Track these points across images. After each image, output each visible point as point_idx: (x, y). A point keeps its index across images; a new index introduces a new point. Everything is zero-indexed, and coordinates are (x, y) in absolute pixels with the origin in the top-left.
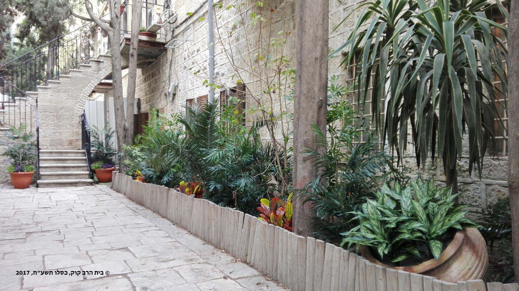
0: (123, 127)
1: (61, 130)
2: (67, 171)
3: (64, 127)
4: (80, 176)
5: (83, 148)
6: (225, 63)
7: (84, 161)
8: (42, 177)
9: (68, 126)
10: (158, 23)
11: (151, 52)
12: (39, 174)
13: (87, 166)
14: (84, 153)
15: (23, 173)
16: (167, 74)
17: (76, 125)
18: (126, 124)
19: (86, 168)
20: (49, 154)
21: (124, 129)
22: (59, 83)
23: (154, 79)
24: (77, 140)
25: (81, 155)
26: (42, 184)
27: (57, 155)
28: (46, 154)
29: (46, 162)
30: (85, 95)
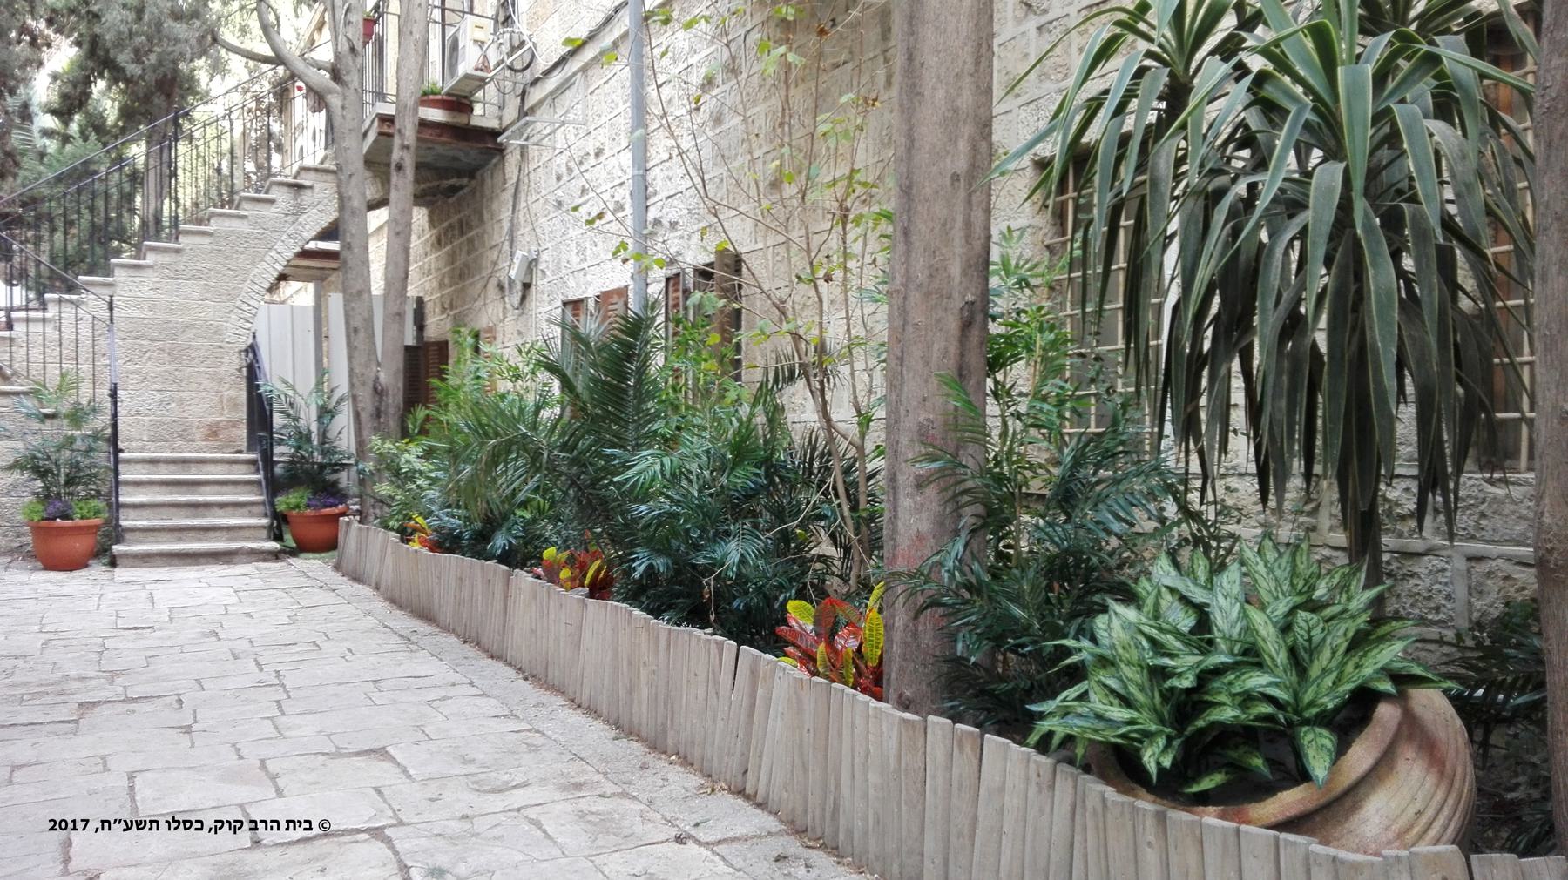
0: (371, 384)
2: (204, 516)
3: (194, 385)
4: (242, 533)
5: (250, 449)
6: (680, 189)
7: (255, 488)
8: (128, 536)
9: (206, 382)
10: (476, 69)
11: (455, 159)
12: (118, 525)
13: (263, 503)
14: (253, 462)
15: (68, 523)
17: (228, 379)
18: (382, 375)
19: (261, 509)
20: (147, 466)
21: (375, 389)
22: (177, 251)
23: (465, 238)
24: (234, 424)
25: (244, 468)
26: (126, 555)
27: (172, 468)
28: (139, 466)
29: (140, 489)
30: (256, 288)
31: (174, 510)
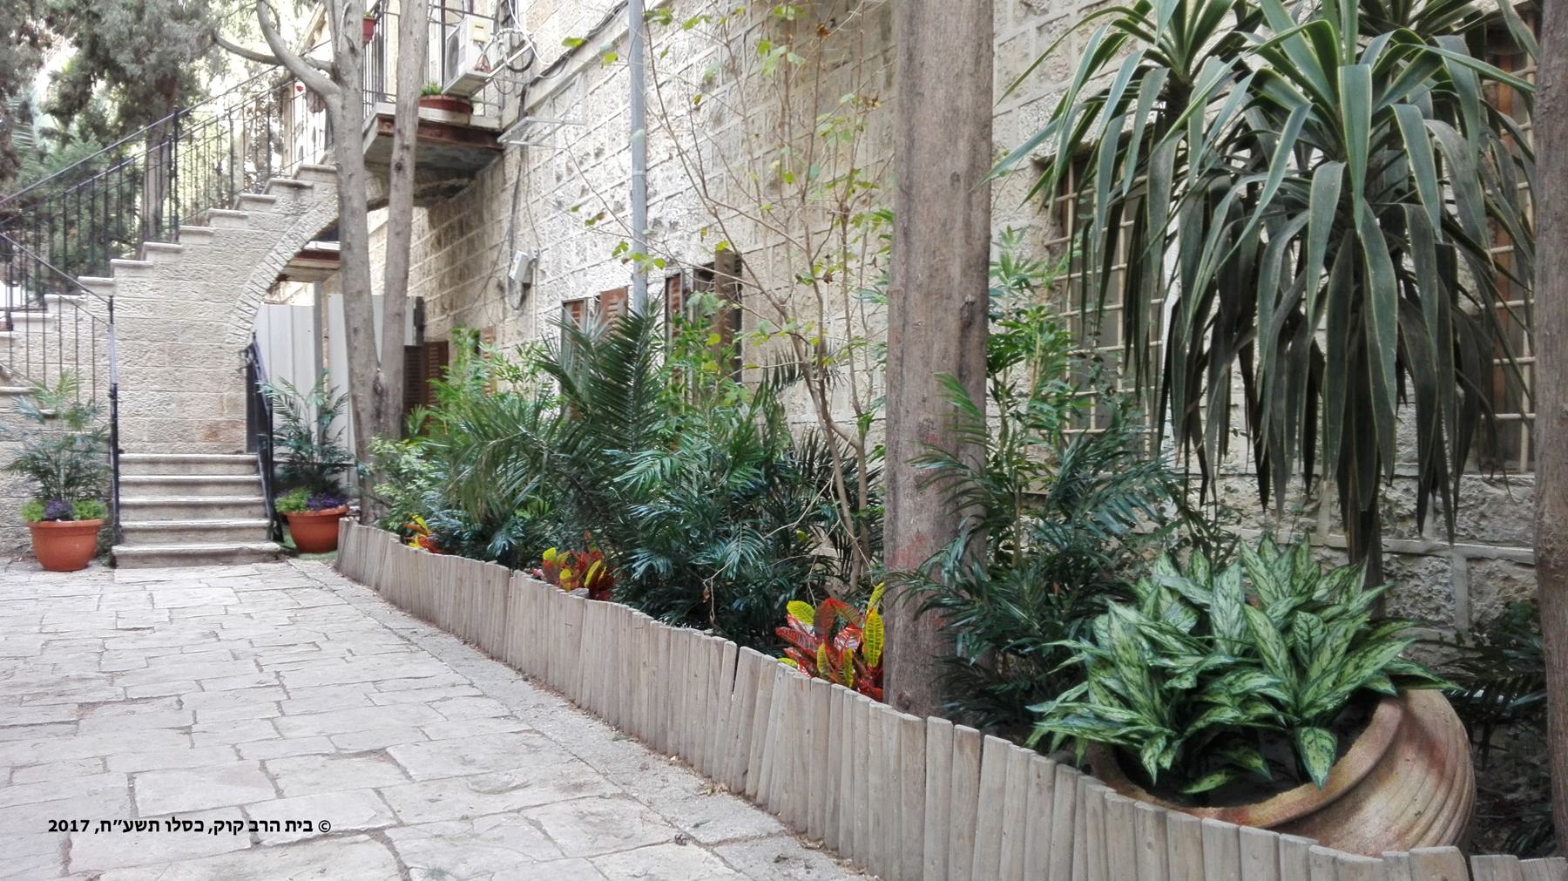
0: (370, 384)
1: (183, 395)
2: (204, 517)
4: (242, 534)
5: (250, 449)
7: (255, 488)
8: (128, 537)
9: (206, 383)
10: (476, 69)
12: (118, 526)
13: (263, 504)
14: (253, 463)
15: (69, 523)
16: (506, 225)
17: (228, 380)
18: (382, 376)
19: (261, 510)
20: (147, 467)
21: (375, 390)
22: (177, 251)
24: (234, 424)
25: (244, 468)
26: (126, 556)
27: (172, 468)
28: (139, 467)
29: (139, 490)
30: (256, 288)
31: (174, 511)
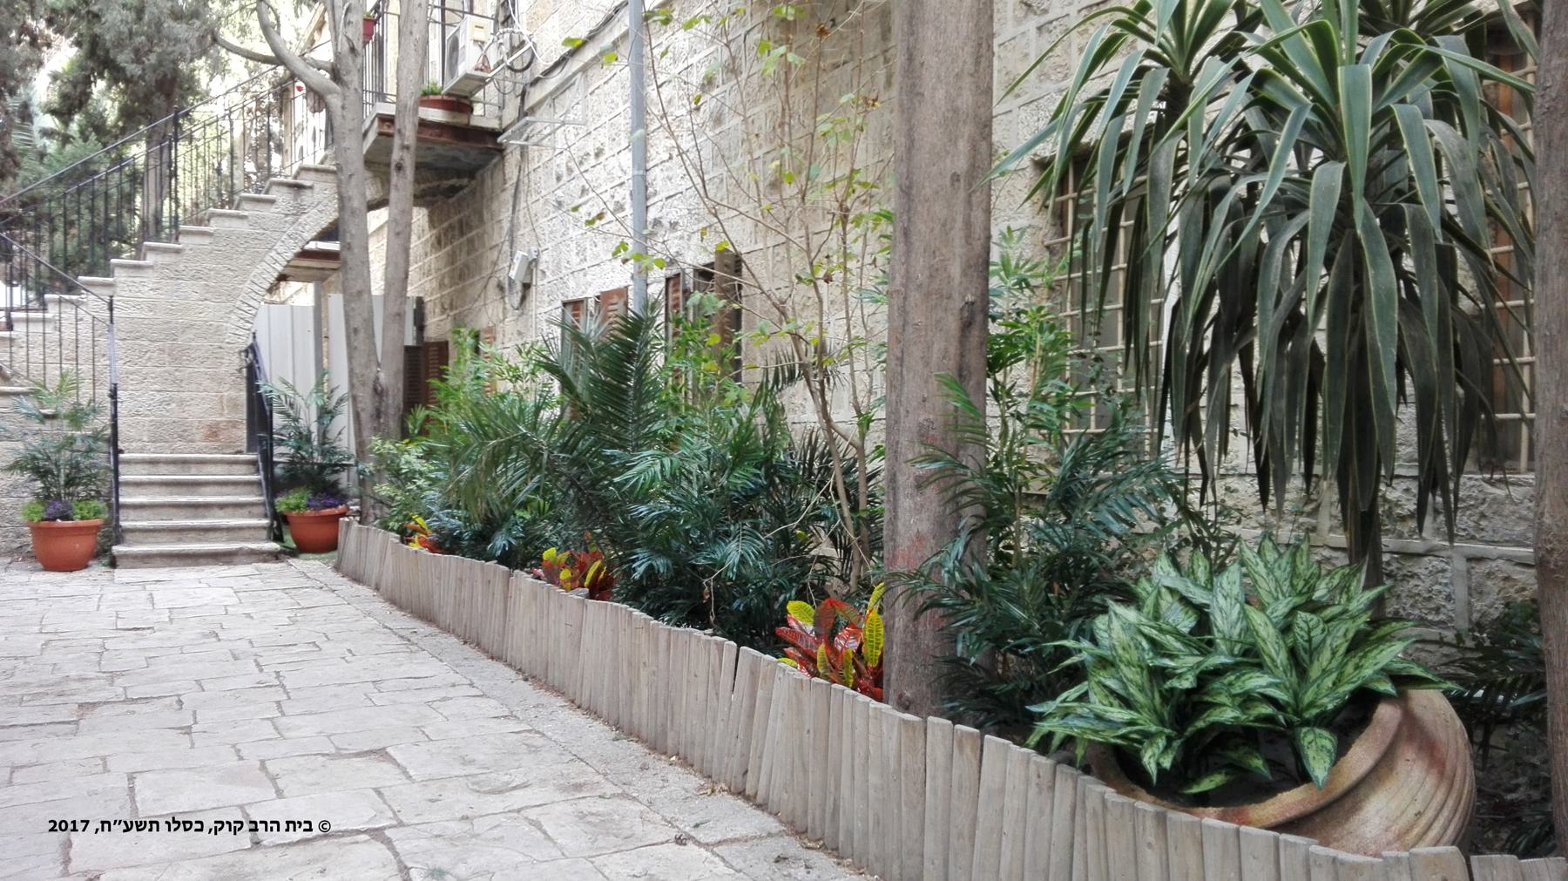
0: (371, 384)
2: (204, 517)
3: (194, 386)
4: (241, 534)
5: (250, 449)
7: (255, 489)
8: (128, 537)
9: (206, 383)
10: (476, 69)
12: (118, 526)
13: (263, 504)
14: (254, 463)
15: (69, 523)
17: (228, 380)
18: (382, 376)
19: (261, 510)
20: (147, 467)
21: (375, 390)
22: (178, 251)
24: (234, 424)
25: (244, 468)
26: (126, 556)
27: (172, 468)
29: (140, 490)
30: (256, 288)
31: (174, 511)
